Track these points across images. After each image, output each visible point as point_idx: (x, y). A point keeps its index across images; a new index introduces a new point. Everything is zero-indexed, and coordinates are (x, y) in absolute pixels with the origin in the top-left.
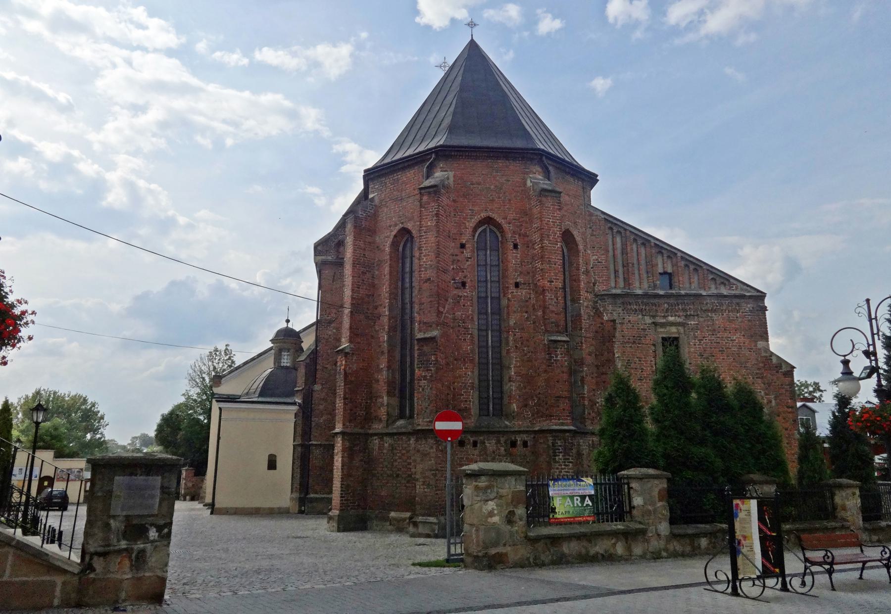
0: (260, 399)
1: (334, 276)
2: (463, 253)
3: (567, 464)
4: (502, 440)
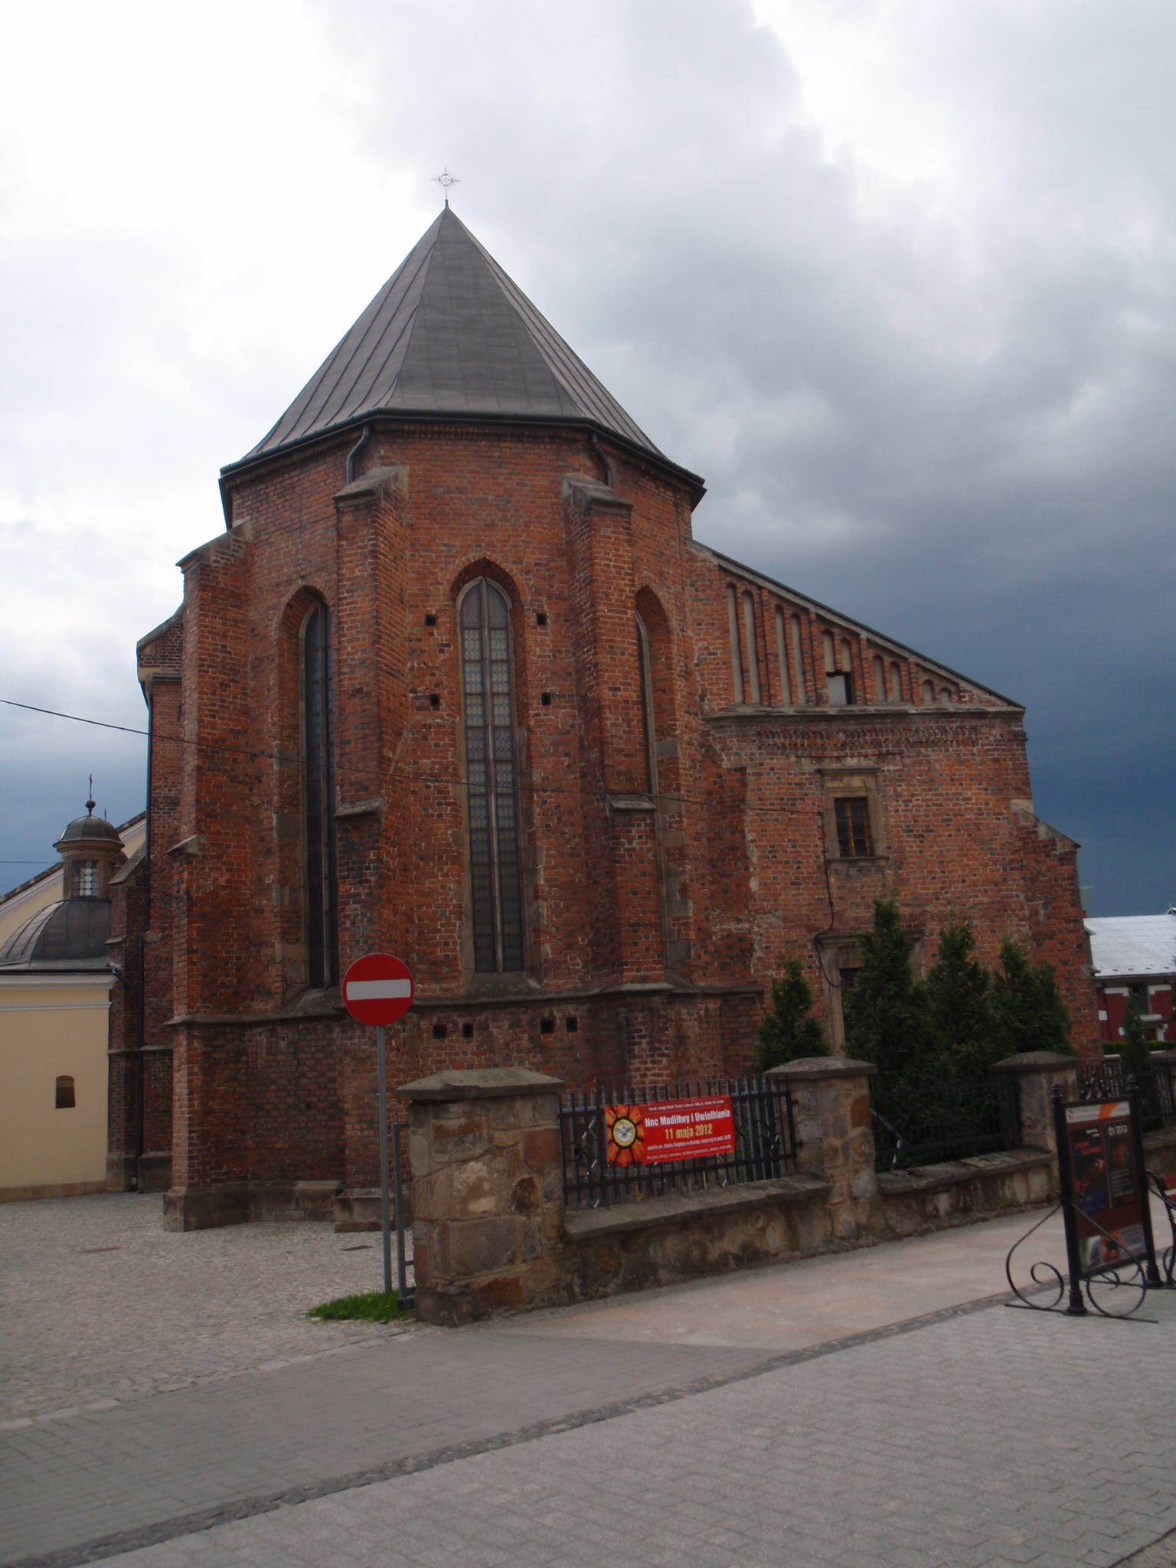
0: (34, 966)
2: (431, 634)
3: (657, 1059)
4: (525, 1018)
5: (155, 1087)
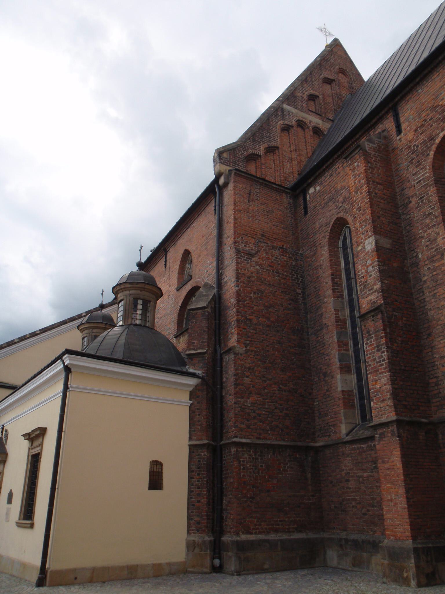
1: (250, 194)
5: (244, 475)
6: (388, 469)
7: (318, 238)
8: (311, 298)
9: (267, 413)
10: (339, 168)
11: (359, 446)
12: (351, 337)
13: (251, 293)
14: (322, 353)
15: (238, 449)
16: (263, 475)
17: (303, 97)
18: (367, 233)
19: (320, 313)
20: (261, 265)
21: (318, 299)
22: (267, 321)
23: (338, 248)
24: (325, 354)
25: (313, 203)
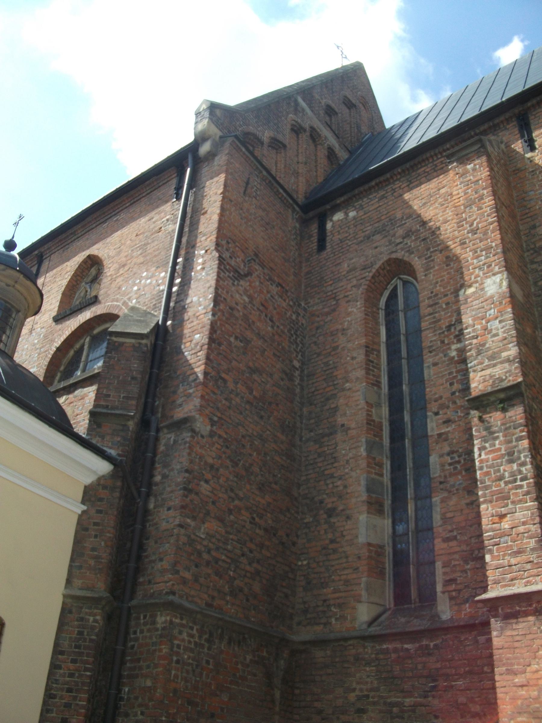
5: (176, 676)
6: (522, 686)
7: (344, 288)
8: (314, 381)
9: (229, 561)
10: (400, 189)
11: (399, 646)
12: (389, 455)
13: (231, 336)
14: (328, 474)
15: (174, 620)
16: (209, 680)
17: (320, 103)
18: (490, 268)
19: (333, 406)
20: (250, 297)
21: (331, 384)
22: (248, 394)
23: (378, 309)
24: (335, 477)
25: (339, 234)
